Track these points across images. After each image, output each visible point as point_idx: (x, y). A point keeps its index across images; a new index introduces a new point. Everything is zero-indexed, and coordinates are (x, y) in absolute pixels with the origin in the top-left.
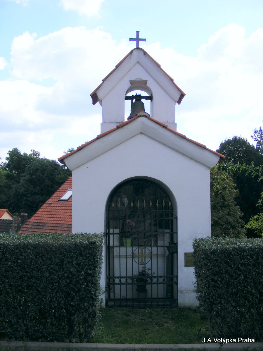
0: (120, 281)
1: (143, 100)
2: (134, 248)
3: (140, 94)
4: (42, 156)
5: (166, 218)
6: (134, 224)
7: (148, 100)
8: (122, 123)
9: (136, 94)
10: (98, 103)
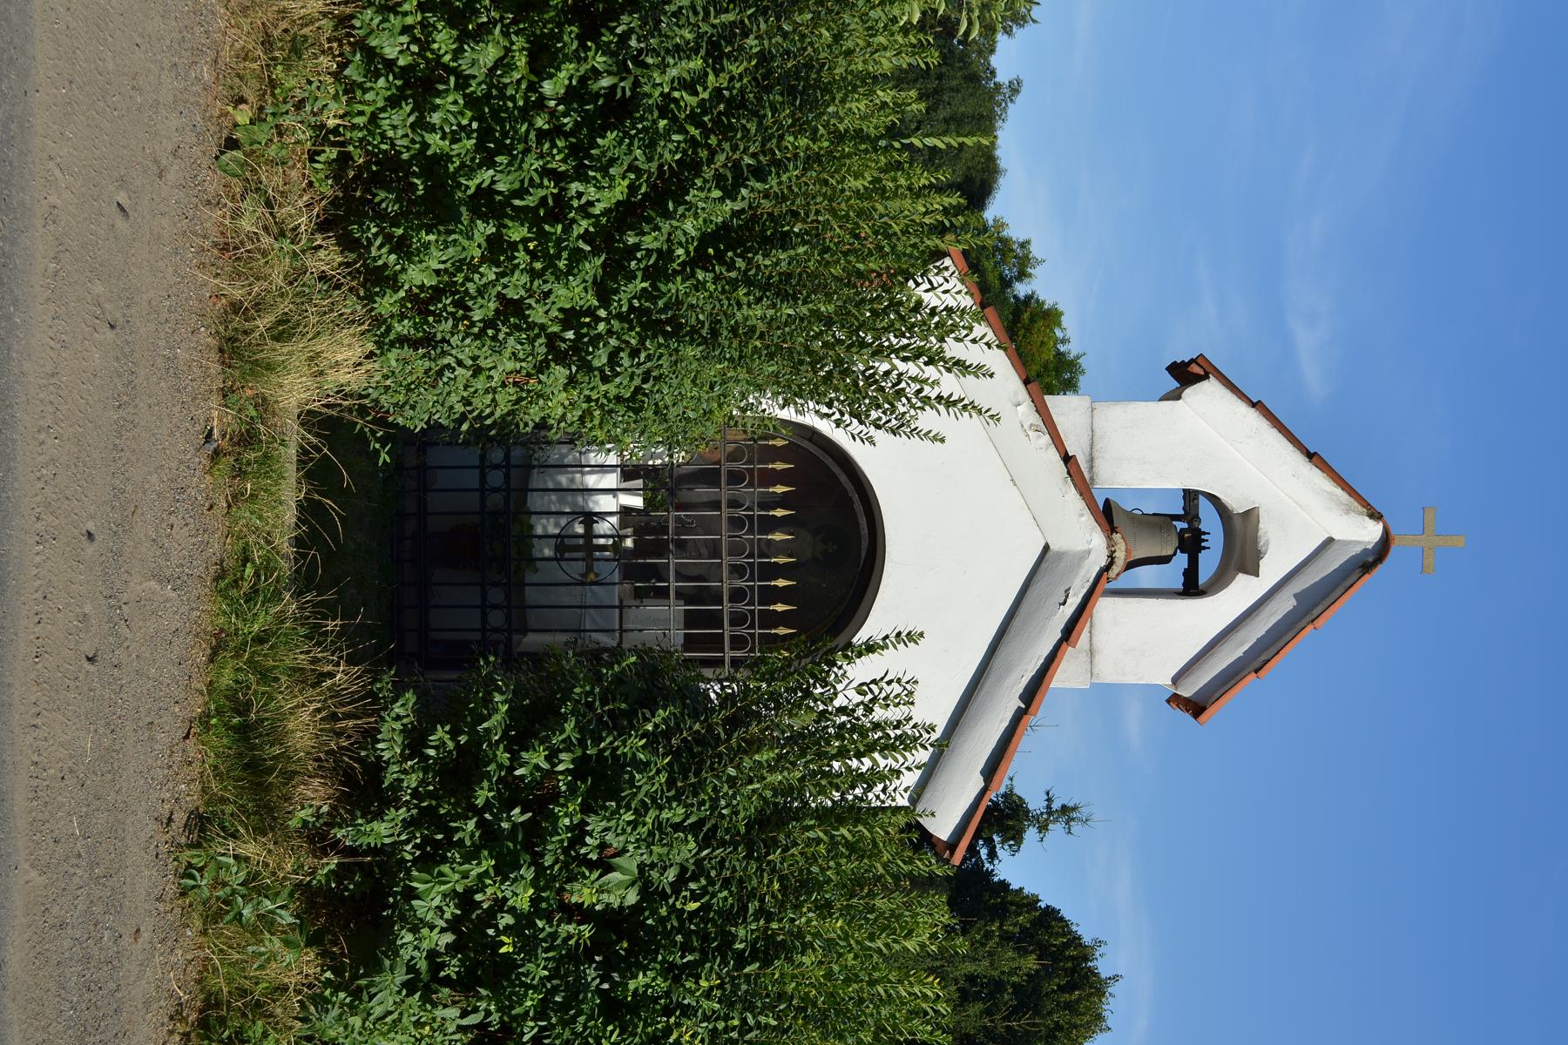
0: (497, 467)
1: (1182, 560)
2: (614, 520)
3: (1205, 548)
4: (1081, 378)
5: (727, 660)
6: (624, 706)
7: (1182, 579)
8: (1092, 479)
9: (1205, 533)
10: (1173, 384)
